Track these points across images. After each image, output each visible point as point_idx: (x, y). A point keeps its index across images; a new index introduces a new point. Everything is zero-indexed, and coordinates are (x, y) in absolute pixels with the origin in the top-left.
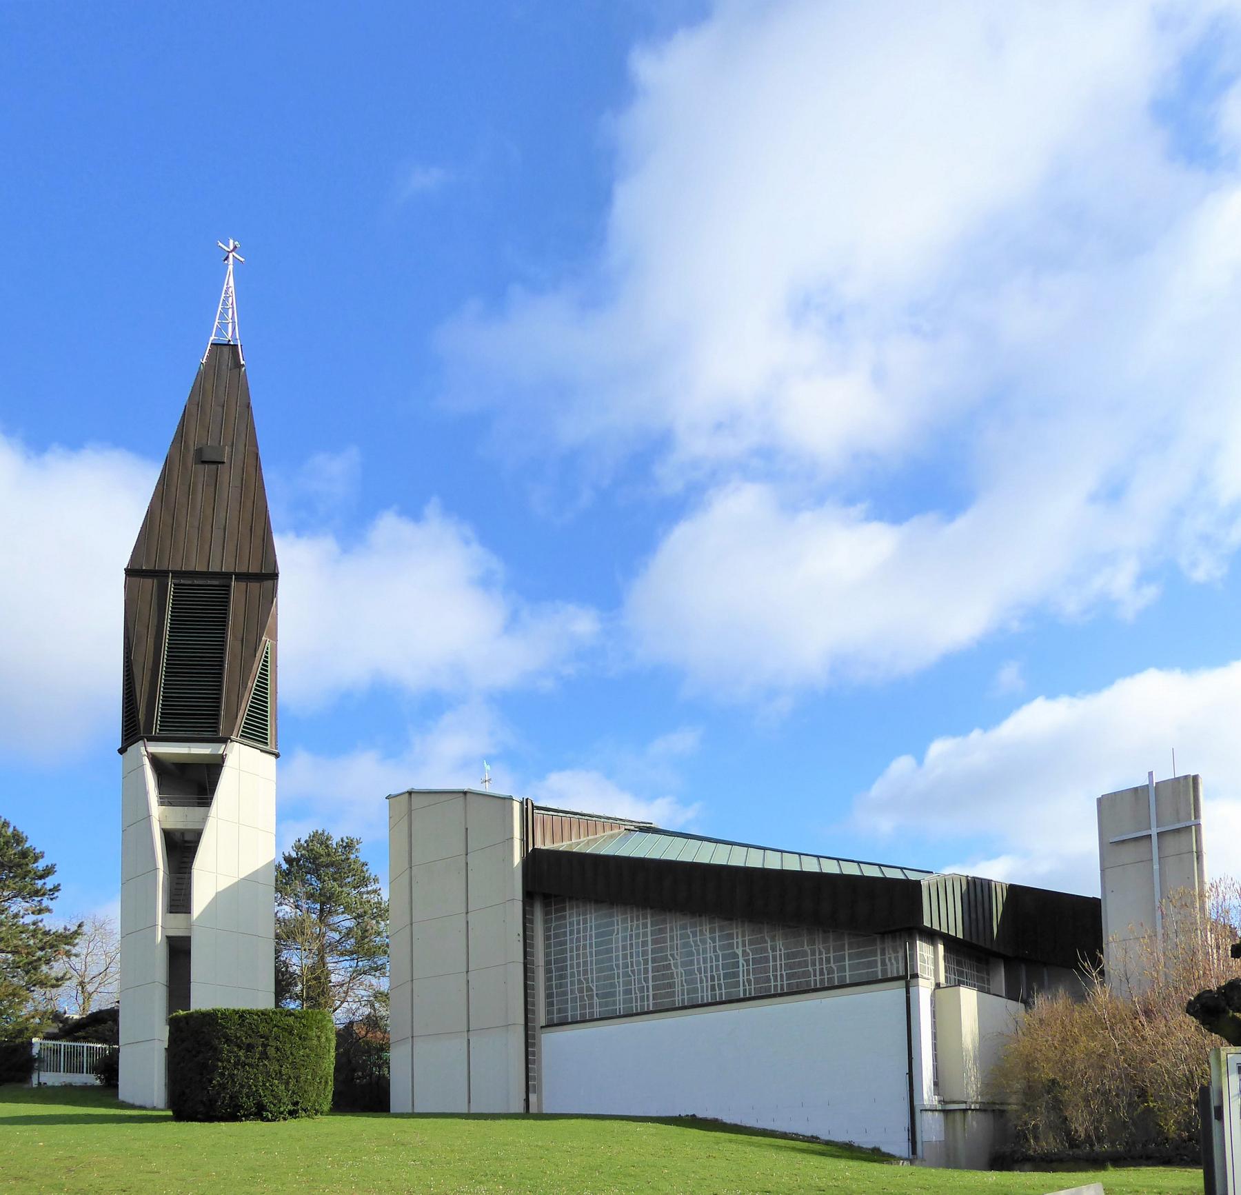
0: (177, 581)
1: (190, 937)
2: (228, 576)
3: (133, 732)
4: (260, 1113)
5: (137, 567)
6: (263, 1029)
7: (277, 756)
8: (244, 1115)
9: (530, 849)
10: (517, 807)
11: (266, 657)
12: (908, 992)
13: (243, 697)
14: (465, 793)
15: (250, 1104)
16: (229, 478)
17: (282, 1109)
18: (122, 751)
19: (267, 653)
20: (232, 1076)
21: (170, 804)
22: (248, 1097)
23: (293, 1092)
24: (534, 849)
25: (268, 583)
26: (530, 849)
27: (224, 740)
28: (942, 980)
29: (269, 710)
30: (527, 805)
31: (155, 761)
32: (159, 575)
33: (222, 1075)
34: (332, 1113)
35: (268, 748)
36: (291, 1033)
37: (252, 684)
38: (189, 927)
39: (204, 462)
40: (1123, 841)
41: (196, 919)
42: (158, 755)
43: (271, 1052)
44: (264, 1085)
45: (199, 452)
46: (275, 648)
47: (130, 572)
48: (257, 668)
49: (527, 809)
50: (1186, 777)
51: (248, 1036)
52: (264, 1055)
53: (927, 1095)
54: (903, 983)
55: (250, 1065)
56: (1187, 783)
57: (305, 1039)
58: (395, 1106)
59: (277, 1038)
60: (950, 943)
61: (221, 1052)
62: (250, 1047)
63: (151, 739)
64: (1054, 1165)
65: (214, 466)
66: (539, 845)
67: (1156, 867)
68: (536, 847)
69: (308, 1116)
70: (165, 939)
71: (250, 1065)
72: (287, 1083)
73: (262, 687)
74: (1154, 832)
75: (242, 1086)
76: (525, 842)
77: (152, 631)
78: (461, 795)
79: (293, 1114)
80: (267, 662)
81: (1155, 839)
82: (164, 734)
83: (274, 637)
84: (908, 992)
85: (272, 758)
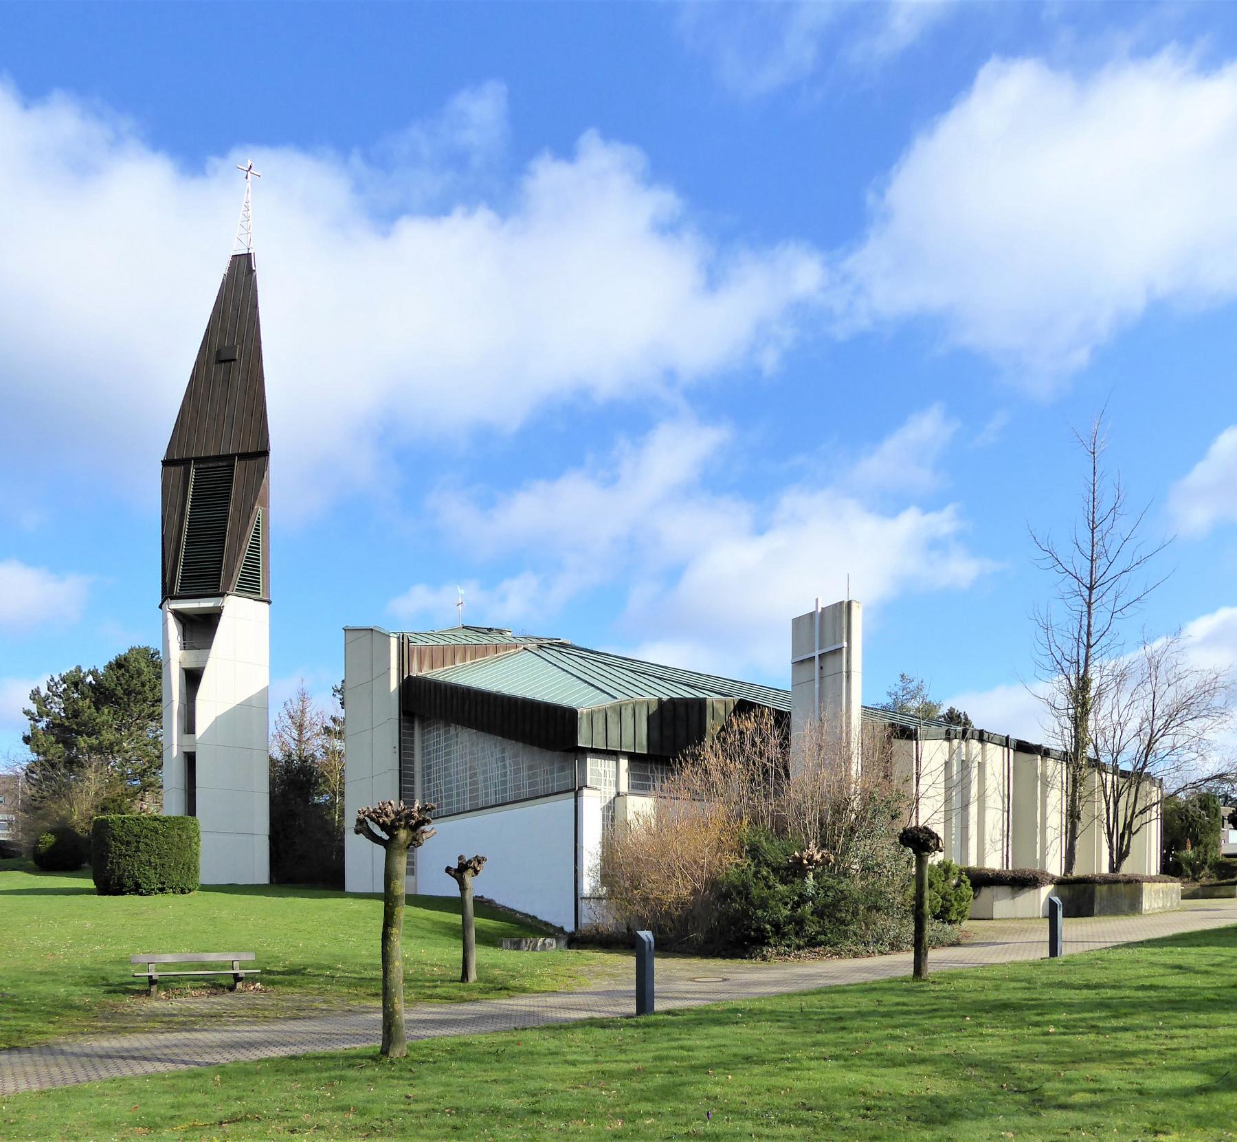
0: (197, 466)
1: (195, 753)
2: (230, 457)
3: (168, 594)
4: (137, 890)
5: (170, 458)
6: (137, 830)
7: (269, 602)
8: (127, 891)
9: (405, 676)
10: (394, 643)
11: (258, 522)
12: (576, 801)
13: (238, 556)
14: (372, 630)
15: (129, 883)
16: (238, 371)
17: (153, 887)
18: (161, 607)
19: (259, 519)
20: (118, 863)
21: (192, 648)
22: (128, 878)
23: (160, 875)
24: (409, 676)
25: (261, 460)
26: (405, 676)
27: (222, 595)
28: (624, 788)
29: (261, 566)
30: (403, 639)
31: (177, 614)
32: (185, 462)
33: (112, 862)
34: (1165, 876)
35: (260, 597)
36: (157, 832)
37: (246, 546)
38: (195, 743)
39: (222, 362)
40: (802, 661)
41: (200, 738)
42: (182, 611)
43: (142, 846)
44: (139, 870)
45: (218, 353)
46: (266, 514)
47: (165, 463)
48: (250, 533)
49: (403, 643)
50: (841, 603)
51: (127, 835)
52: (138, 849)
53: (588, 884)
54: (573, 794)
55: (130, 857)
56: (841, 608)
57: (167, 837)
58: (350, 886)
59: (146, 837)
60: (632, 757)
61: (111, 847)
62: (128, 843)
63: (173, 598)
64: (586, 945)
65: (228, 364)
66: (414, 674)
67: (817, 686)
68: (411, 674)
69: (174, 892)
70: (182, 756)
71: (130, 857)
72: (156, 869)
73: (255, 548)
74: (817, 653)
75: (125, 871)
76: (401, 670)
77: (178, 509)
78: (370, 631)
79: (162, 890)
80: (259, 526)
81: (817, 658)
82: (183, 593)
83: (265, 504)
84: (576, 801)
85: (266, 605)
